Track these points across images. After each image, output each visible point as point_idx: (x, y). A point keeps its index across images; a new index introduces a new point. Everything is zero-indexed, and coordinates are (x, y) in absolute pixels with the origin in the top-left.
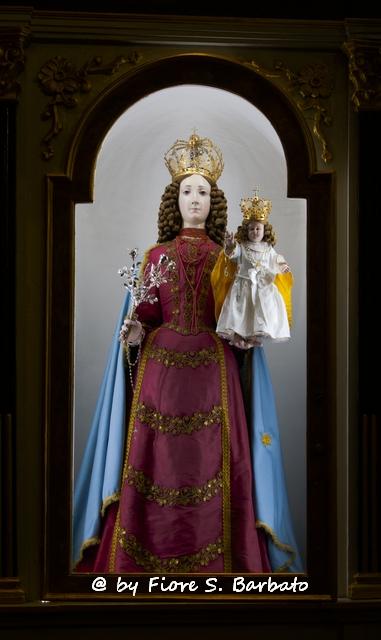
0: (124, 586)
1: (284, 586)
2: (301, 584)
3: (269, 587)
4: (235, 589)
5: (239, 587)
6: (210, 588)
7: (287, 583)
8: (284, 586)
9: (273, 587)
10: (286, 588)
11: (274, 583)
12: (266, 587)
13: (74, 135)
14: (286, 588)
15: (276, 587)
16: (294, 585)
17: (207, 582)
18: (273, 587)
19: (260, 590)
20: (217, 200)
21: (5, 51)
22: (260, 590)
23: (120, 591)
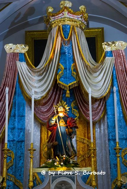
2: (103, 172)
3: (94, 173)
15: (96, 173)
16: (101, 173)
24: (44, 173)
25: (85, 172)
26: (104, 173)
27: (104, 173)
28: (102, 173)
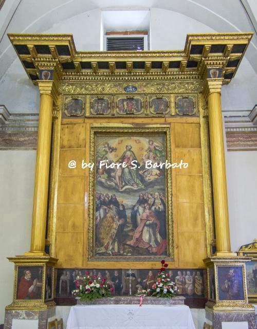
0: (169, 165)
1: (175, 165)
2: (185, 164)
4: (146, 167)
5: (149, 166)
6: (133, 166)
7: (176, 164)
8: (175, 165)
9: (85, 165)
10: (176, 166)
11: (86, 164)
12: (164, 165)
13: (203, 205)
14: (176, 166)
16: (180, 164)
17: (187, 164)
18: (85, 165)
19: (161, 168)
20: (188, 244)
21: (191, 296)
23: (84, 168)
24: (74, 165)
25: (150, 164)
28: (182, 166)
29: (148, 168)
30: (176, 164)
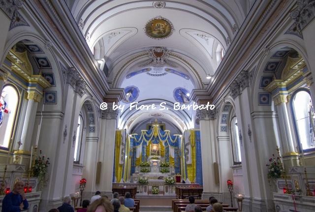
1: (202, 107)
2: (211, 106)
3: (194, 107)
7: (203, 105)
9: (196, 107)
10: (203, 108)
15: (197, 108)
22: (189, 109)
26: (213, 107)
27: (213, 107)
28: (209, 107)
29: (176, 110)
30: (203, 105)
